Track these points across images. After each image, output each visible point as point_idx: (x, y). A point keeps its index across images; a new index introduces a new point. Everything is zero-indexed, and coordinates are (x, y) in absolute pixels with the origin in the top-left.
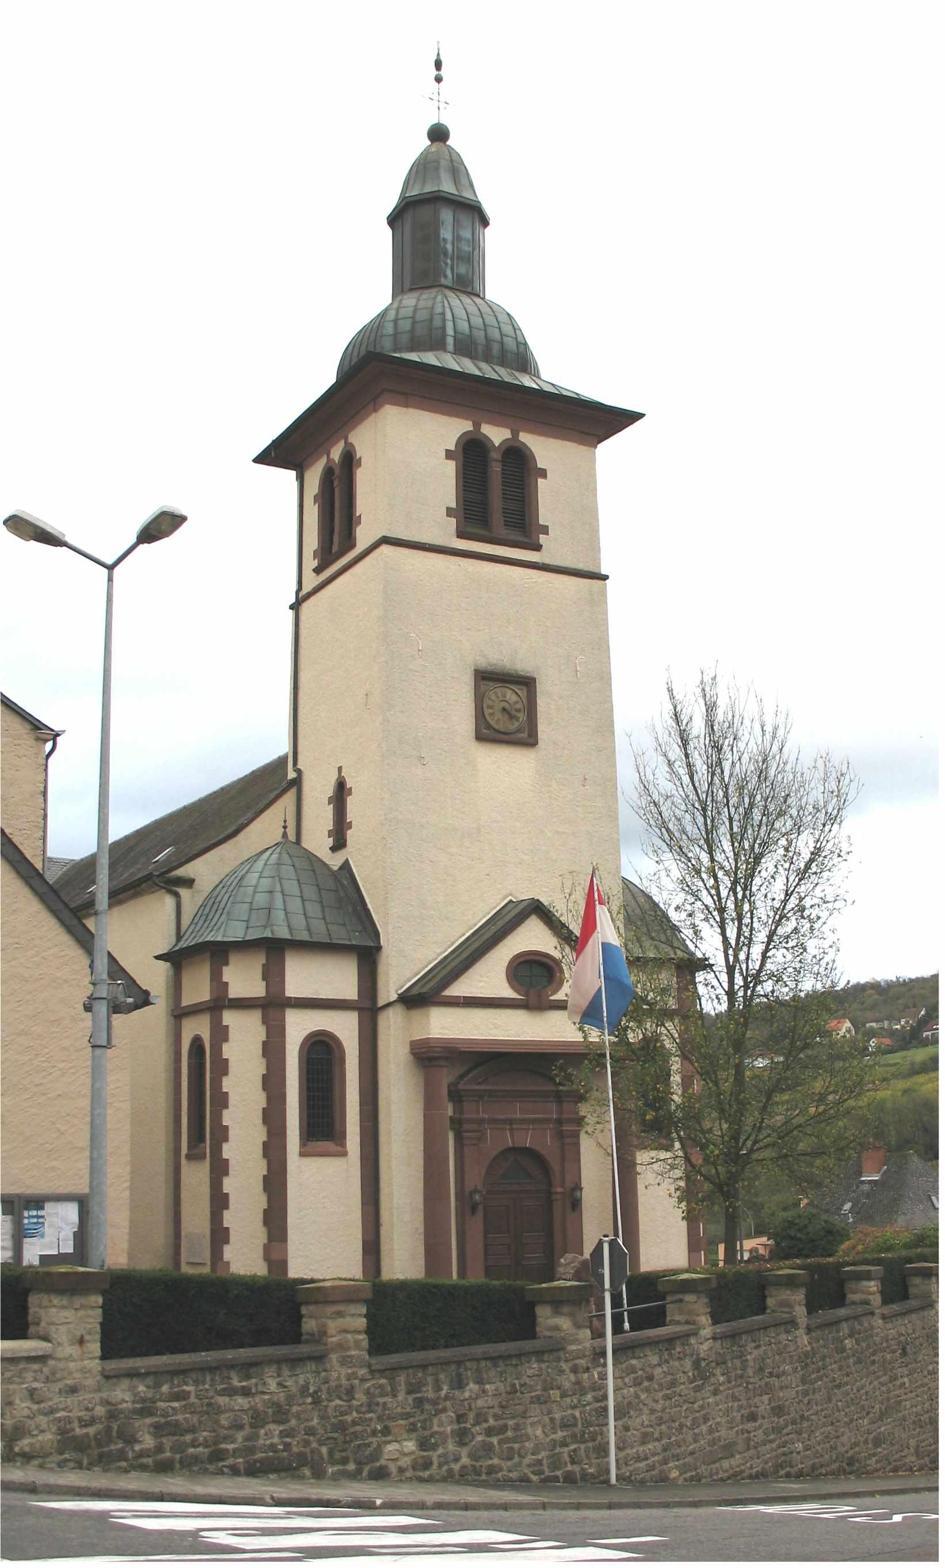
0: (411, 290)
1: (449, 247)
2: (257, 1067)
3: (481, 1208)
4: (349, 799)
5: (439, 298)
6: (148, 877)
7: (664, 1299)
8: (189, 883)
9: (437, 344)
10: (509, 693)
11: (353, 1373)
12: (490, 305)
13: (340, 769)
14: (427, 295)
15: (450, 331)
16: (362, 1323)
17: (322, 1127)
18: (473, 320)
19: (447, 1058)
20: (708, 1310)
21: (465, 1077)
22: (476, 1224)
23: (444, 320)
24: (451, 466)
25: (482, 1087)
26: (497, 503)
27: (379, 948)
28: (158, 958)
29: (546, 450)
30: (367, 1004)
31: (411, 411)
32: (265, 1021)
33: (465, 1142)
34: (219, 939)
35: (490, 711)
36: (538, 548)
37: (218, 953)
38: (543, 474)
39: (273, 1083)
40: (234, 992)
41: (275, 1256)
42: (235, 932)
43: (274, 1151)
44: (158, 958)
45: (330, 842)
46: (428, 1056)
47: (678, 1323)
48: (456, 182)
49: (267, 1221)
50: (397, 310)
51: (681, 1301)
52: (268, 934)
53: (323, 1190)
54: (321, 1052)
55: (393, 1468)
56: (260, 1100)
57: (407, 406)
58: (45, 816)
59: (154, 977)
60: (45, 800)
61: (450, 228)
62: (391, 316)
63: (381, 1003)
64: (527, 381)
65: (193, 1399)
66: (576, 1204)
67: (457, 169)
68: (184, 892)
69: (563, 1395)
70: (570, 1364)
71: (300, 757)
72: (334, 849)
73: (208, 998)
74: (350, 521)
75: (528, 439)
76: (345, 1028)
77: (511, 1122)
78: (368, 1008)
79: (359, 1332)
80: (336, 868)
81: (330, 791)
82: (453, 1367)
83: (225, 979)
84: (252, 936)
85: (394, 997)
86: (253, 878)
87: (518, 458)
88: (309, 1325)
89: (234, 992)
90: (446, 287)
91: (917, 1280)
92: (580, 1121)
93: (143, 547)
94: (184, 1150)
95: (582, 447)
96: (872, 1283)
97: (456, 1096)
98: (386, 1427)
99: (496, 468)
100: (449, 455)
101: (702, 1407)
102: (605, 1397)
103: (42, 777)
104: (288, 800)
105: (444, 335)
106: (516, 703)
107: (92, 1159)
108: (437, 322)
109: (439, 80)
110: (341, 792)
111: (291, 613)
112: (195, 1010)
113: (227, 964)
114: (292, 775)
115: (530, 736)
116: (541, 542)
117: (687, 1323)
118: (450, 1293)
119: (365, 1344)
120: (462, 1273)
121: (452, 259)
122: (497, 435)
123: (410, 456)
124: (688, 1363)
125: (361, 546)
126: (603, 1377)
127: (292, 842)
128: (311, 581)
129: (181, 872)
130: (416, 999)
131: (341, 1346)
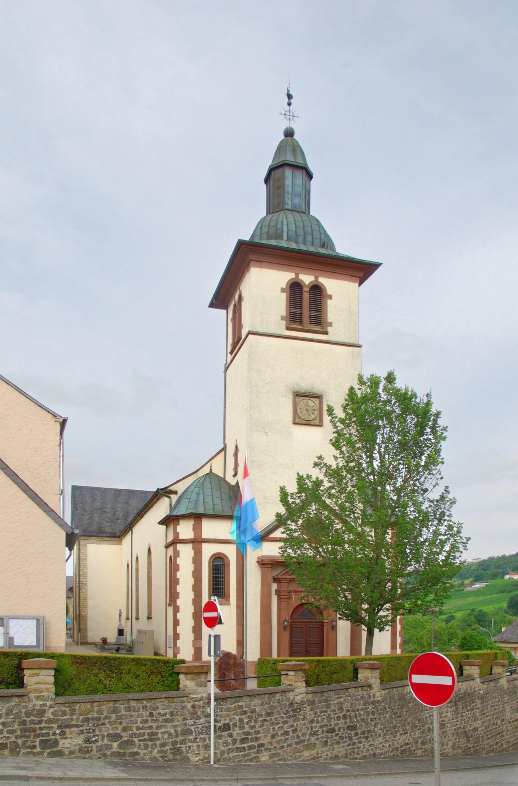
1: (290, 189)
8: (176, 493)
9: (279, 237)
19: (271, 564)
20: (304, 679)
23: (282, 224)
24: (283, 297)
26: (306, 311)
31: (263, 269)
34: (175, 514)
35: (300, 411)
36: (326, 333)
38: (330, 297)
40: (181, 537)
41: (198, 646)
46: (265, 563)
48: (295, 155)
49: (194, 631)
51: (287, 674)
55: (66, 752)
57: (261, 268)
61: (291, 180)
67: (296, 149)
82: (112, 704)
87: (317, 290)
94: (168, 602)
98: (62, 732)
99: (306, 296)
100: (283, 290)
106: (314, 406)
108: (279, 226)
113: (179, 525)
115: (320, 422)
116: (328, 330)
118: (398, 659)
119: (54, 689)
120: (279, 655)
121: (292, 195)
122: (307, 279)
125: (243, 337)
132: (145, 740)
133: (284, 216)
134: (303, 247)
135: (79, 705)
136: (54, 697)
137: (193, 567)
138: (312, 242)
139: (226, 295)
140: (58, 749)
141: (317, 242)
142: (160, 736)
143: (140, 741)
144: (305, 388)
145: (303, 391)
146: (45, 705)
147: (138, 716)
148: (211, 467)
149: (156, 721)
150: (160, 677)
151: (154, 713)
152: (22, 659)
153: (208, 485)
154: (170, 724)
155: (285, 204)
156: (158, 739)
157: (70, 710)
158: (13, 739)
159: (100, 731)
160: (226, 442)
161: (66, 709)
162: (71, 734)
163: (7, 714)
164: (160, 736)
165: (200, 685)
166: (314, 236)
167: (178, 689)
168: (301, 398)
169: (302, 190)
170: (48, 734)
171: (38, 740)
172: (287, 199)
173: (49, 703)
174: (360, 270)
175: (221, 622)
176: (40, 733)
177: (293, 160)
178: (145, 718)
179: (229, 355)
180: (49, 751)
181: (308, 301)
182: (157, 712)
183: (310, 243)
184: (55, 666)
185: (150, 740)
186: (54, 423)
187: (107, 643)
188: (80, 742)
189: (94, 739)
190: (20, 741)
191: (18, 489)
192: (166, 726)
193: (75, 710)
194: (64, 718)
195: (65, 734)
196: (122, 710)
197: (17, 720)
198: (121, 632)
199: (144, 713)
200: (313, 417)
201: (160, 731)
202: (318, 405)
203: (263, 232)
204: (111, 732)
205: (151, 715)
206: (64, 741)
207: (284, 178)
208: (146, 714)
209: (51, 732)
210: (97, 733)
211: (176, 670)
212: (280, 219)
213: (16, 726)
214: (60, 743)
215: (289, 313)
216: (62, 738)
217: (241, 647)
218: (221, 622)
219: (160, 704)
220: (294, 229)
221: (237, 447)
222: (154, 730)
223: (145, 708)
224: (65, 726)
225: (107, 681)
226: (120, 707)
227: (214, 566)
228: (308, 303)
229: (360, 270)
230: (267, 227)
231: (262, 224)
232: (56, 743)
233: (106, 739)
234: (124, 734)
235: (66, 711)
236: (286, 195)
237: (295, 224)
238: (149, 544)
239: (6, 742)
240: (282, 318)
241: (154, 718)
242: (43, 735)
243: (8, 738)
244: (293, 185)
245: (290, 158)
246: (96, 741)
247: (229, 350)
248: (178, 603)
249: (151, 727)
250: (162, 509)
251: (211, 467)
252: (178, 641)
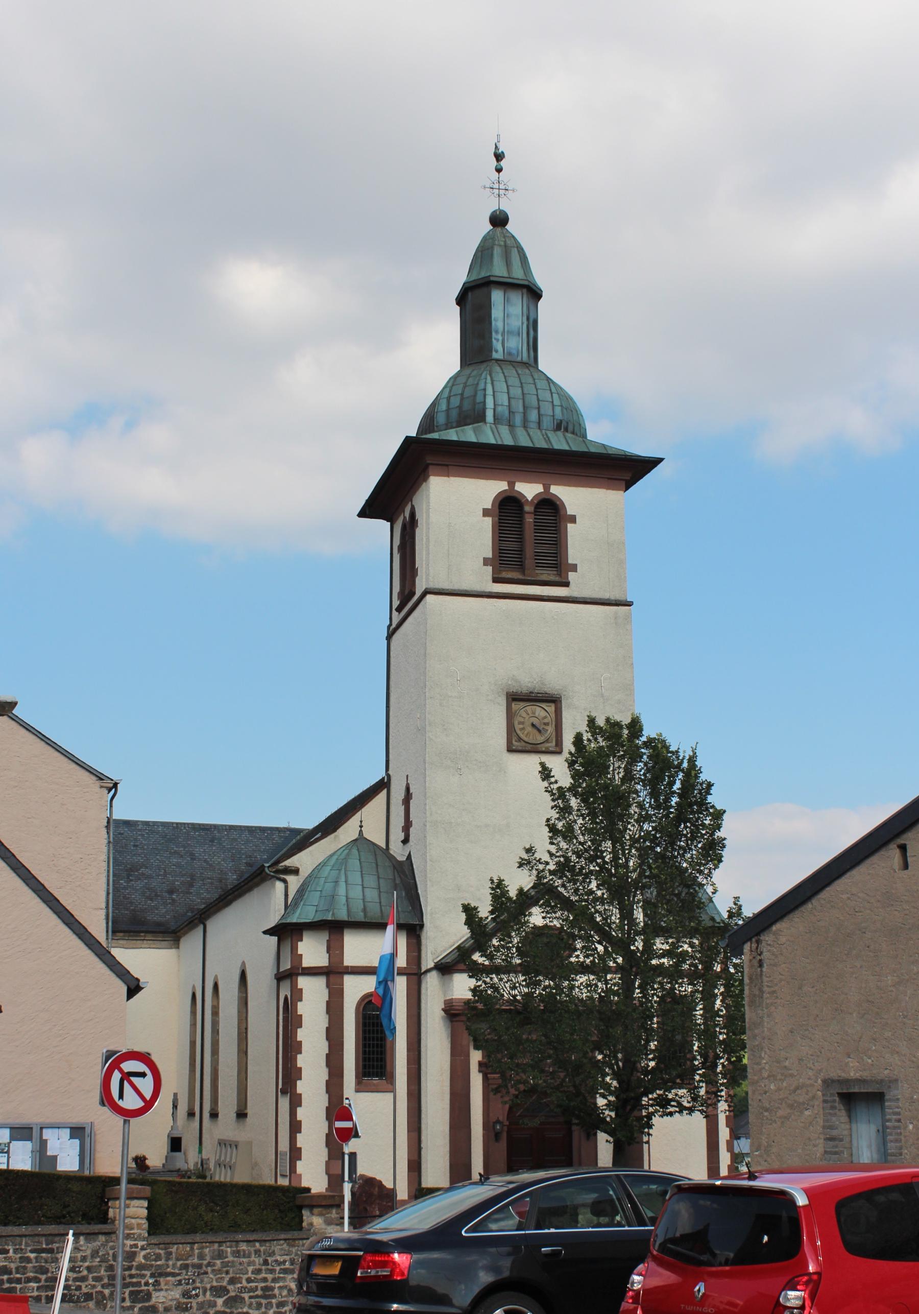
2: (322, 1021)
8: (296, 872)
10: (538, 709)
17: (375, 1066)
23: (485, 396)
24: (489, 521)
26: (529, 547)
27: (422, 926)
31: (452, 479)
34: (295, 921)
35: (521, 726)
36: (567, 584)
38: (573, 519)
39: (334, 1035)
40: (306, 963)
43: (334, 1085)
52: (330, 917)
53: (376, 1114)
61: (501, 308)
62: (446, 395)
65: (11, 1253)
68: (290, 878)
75: (557, 490)
82: (216, 1245)
85: (431, 965)
87: (549, 507)
94: (280, 1086)
98: (156, 1281)
100: (486, 512)
106: (545, 717)
108: (479, 398)
113: (302, 940)
115: (557, 745)
119: (146, 1226)
122: (529, 490)
129: (288, 863)
130: (445, 969)
132: (257, 1297)
133: (489, 378)
135: (176, 1246)
136: (146, 1235)
137: (327, 1020)
138: (539, 423)
139: (392, 497)
140: (150, 1303)
142: (276, 1291)
143: (251, 1297)
144: (529, 685)
145: (525, 690)
146: (136, 1246)
147: (249, 1264)
148: (361, 827)
149: (272, 1271)
150: (277, 1211)
151: (270, 1260)
152: (105, 1186)
153: (354, 863)
154: (290, 1276)
155: (491, 352)
156: (274, 1296)
157: (165, 1253)
158: (99, 1288)
159: (202, 1282)
160: (390, 772)
161: (161, 1251)
162: (166, 1284)
163: (93, 1256)
164: (276, 1291)
165: (329, 1222)
166: (542, 412)
167: (301, 1228)
168: (522, 704)
169: (522, 323)
170: (138, 1284)
171: (127, 1291)
172: (494, 341)
173: (140, 1244)
174: (626, 470)
175: (357, 1135)
176: (130, 1283)
177: (505, 274)
178: (258, 1267)
179: (395, 613)
180: (140, 1305)
181: (532, 527)
182: (274, 1258)
183: (533, 425)
184: (148, 1194)
185: (265, 1297)
186: (98, 789)
187: (147, 1167)
188: (178, 1296)
189: (194, 1292)
190: (107, 1292)
191: (59, 921)
192: (284, 1279)
193: (171, 1253)
194: (159, 1263)
195: (159, 1284)
196: (229, 1254)
197: (104, 1264)
198: (175, 1144)
199: (257, 1260)
201: (277, 1285)
202: (553, 716)
203: (451, 406)
204: (215, 1284)
205: (266, 1262)
206: (158, 1294)
208: (258, 1261)
209: (143, 1282)
210: (198, 1285)
211: (298, 1202)
212: (481, 386)
213: (103, 1272)
214: (153, 1296)
215: (498, 551)
216: (155, 1290)
217: (416, 1174)
218: (357, 1135)
219: (277, 1247)
220: (506, 403)
221: (408, 789)
222: (269, 1284)
223: (257, 1252)
224: (159, 1274)
225: (208, 1217)
226: (227, 1252)
227: (365, 1017)
228: (533, 531)
229: (626, 470)
230: (458, 398)
231: (450, 391)
232: (149, 1296)
233: (208, 1293)
234: (230, 1287)
235: (160, 1254)
236: (493, 334)
237: (508, 393)
238: (243, 963)
239: (91, 1291)
240: (486, 562)
241: (270, 1267)
242: (133, 1285)
243: (94, 1287)
244: (506, 316)
245: (498, 270)
246: (197, 1295)
247: (396, 603)
248: (299, 1090)
249: (265, 1280)
250: (272, 903)
251: (361, 827)
252: (298, 1163)
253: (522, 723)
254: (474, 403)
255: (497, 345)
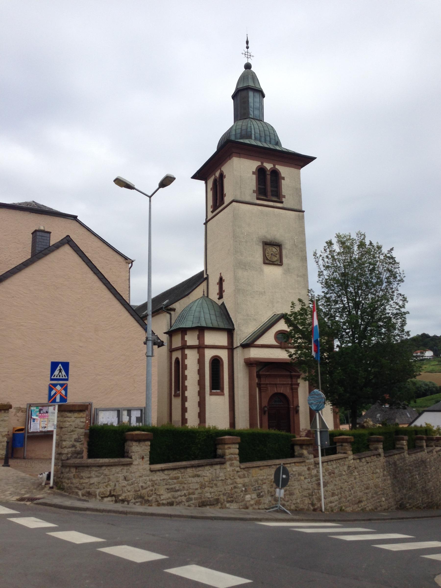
0: (240, 120)
3: (267, 412)
4: (224, 283)
5: (249, 122)
6: (162, 308)
7: (336, 444)
9: (250, 137)
11: (235, 469)
12: (265, 123)
13: (221, 273)
14: (245, 121)
15: (253, 133)
16: (237, 451)
18: (260, 128)
21: (262, 370)
22: (266, 418)
23: (251, 129)
24: (254, 177)
25: (267, 373)
26: (269, 188)
27: (234, 329)
28: (165, 333)
29: (284, 171)
30: (231, 347)
32: (198, 352)
33: (262, 391)
34: (184, 327)
36: (282, 202)
37: (184, 331)
38: (283, 178)
39: (201, 372)
40: (189, 344)
42: (188, 324)
43: (201, 394)
44: (165, 333)
45: (218, 296)
47: (341, 453)
48: (254, 82)
50: (236, 126)
54: (216, 362)
56: (197, 377)
58: (129, 287)
59: (164, 338)
60: (129, 282)
62: (234, 128)
63: (235, 346)
64: (278, 148)
66: (297, 412)
67: (254, 77)
68: (172, 313)
69: (305, 478)
70: (307, 467)
71: (208, 271)
72: (219, 299)
73: (180, 345)
74: (222, 195)
76: (224, 355)
77: (276, 384)
78: (231, 348)
79: (235, 454)
80: (220, 305)
81: (218, 280)
83: (186, 339)
84: (194, 325)
85: (239, 345)
86: (194, 308)
87: (275, 174)
88: (219, 452)
89: (189, 344)
90: (252, 118)
91: (418, 441)
92: (298, 384)
93: (161, 189)
95: (296, 169)
96: (404, 442)
97: (259, 376)
99: (269, 177)
100: (254, 173)
101: (351, 484)
102: (319, 479)
103: (128, 275)
104: (205, 283)
105: (251, 135)
107: (147, 395)
109: (247, 48)
110: (221, 281)
111: (204, 226)
112: (177, 349)
113: (186, 335)
114: (205, 276)
117: (344, 453)
119: (238, 459)
122: (268, 166)
123: (241, 172)
124: (346, 468)
125: (226, 203)
126: (318, 472)
127: (206, 296)
128: (210, 215)
129: (171, 307)
131: (231, 459)
134: (266, 146)
137: (198, 367)
141: (273, 141)
166: (271, 138)
172: (250, 111)
183: (268, 142)
200: (276, 259)
207: (248, 97)
253: (268, 253)
254: (247, 132)
255: (251, 113)
